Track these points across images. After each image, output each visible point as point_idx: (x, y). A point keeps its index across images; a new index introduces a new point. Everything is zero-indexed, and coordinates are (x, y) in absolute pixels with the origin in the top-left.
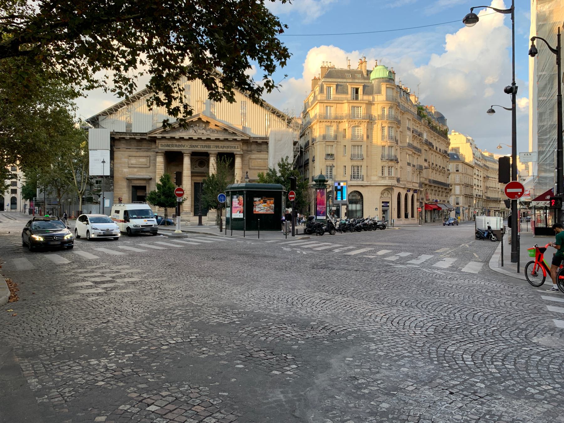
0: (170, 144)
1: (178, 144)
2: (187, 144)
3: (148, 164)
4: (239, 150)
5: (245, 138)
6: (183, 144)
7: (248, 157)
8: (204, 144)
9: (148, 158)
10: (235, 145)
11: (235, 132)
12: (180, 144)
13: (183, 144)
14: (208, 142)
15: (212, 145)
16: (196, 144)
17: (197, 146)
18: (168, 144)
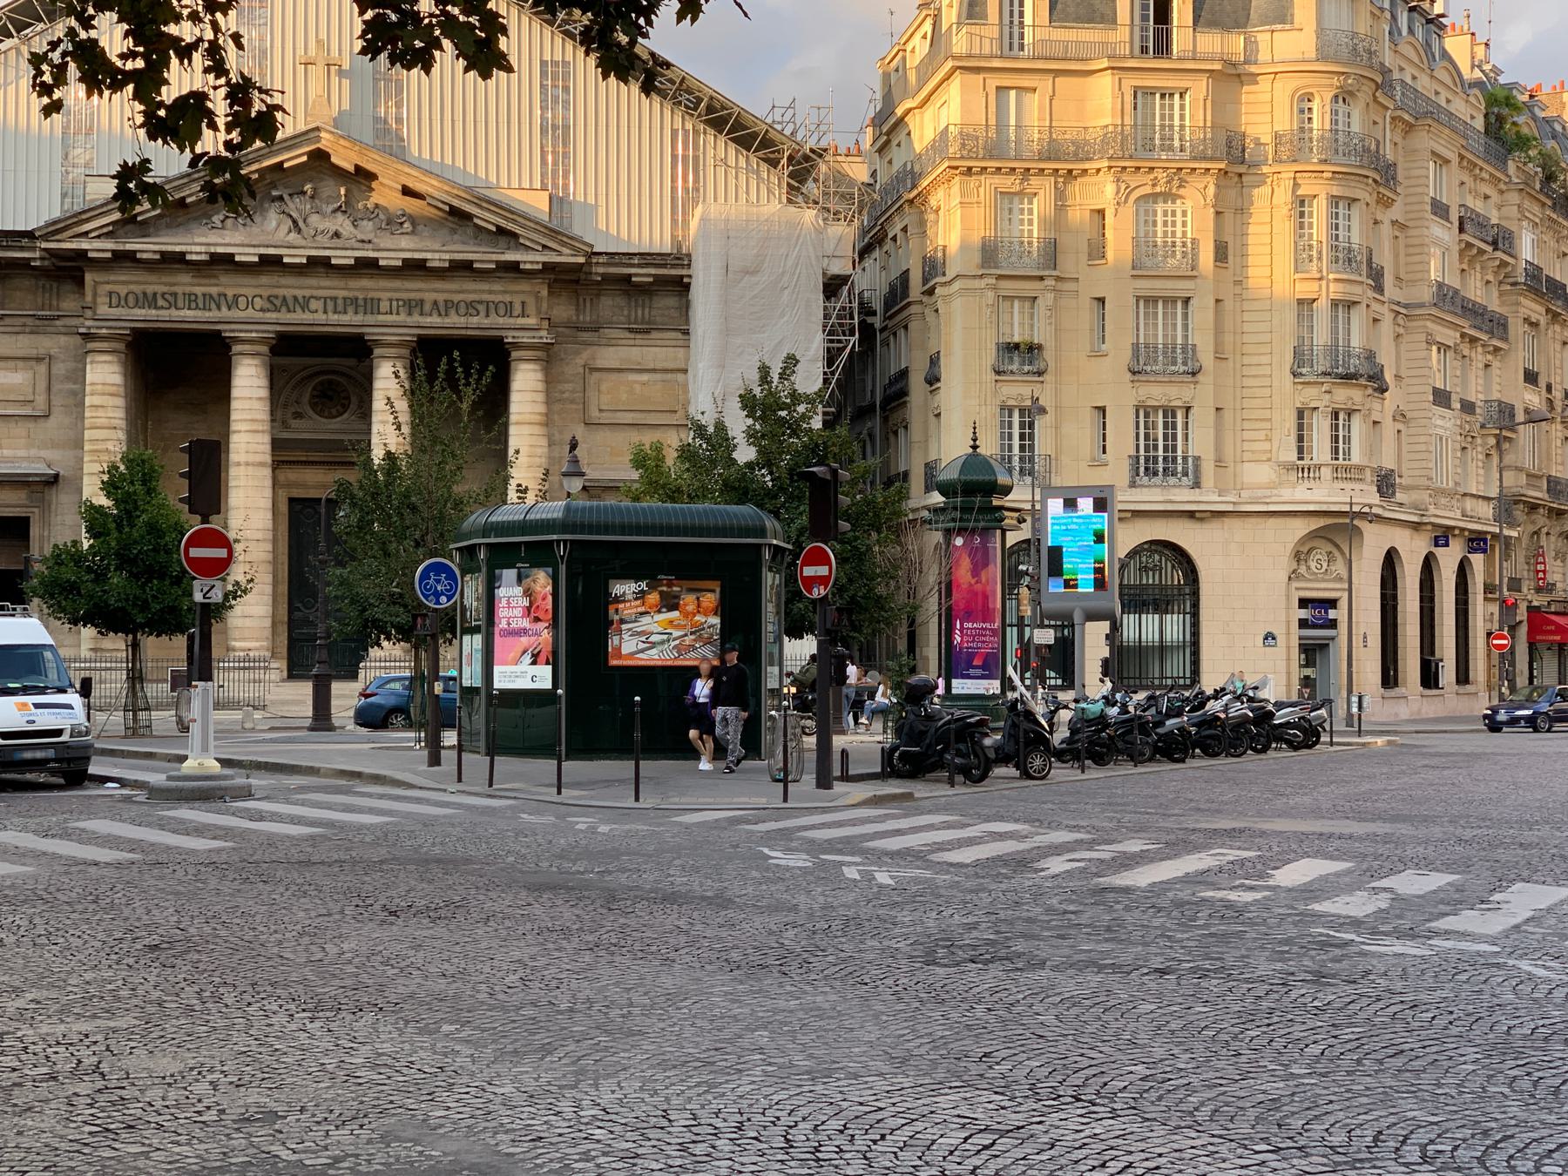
0: (161, 289)
1: (199, 290)
2: (250, 292)
3: (41, 400)
4: (531, 321)
5: (567, 257)
6: (230, 293)
7: (580, 361)
8: (342, 294)
9: (42, 369)
10: (507, 298)
11: (510, 226)
12: (214, 290)
13: (230, 293)
14: (365, 283)
15: (385, 295)
16: (299, 293)
17: (307, 300)
18: (150, 289)
